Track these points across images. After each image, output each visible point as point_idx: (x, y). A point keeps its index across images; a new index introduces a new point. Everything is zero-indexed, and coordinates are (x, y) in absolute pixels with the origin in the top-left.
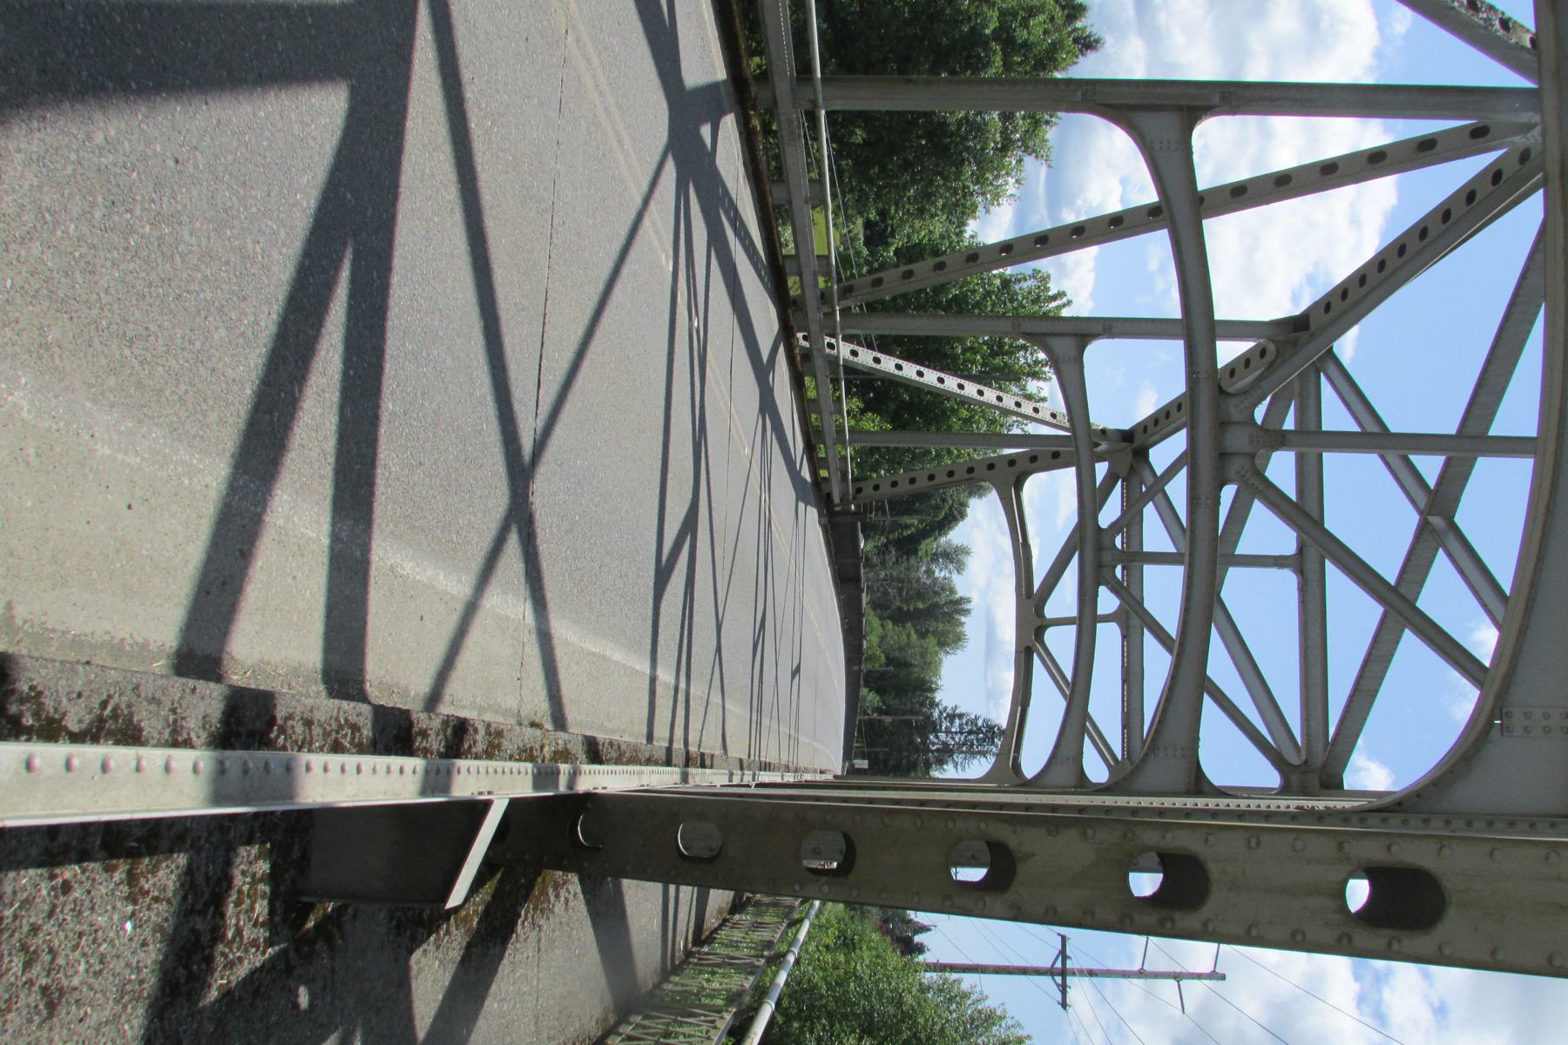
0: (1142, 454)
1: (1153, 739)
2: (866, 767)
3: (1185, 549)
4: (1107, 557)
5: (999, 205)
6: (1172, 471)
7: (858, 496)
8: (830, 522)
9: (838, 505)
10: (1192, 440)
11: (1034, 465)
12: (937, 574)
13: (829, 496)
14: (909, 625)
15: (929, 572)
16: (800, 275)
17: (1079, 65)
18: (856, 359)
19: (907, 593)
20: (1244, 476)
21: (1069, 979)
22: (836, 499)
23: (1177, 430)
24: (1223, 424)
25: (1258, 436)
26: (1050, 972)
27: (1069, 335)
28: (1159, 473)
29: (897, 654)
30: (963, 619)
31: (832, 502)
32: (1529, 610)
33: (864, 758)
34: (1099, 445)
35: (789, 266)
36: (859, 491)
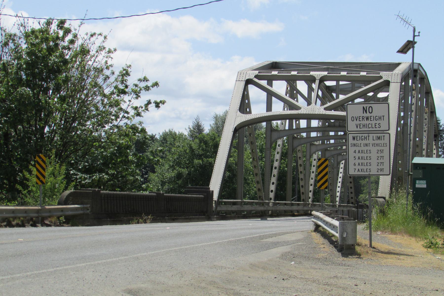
7: (354, 203)
36: (352, 203)
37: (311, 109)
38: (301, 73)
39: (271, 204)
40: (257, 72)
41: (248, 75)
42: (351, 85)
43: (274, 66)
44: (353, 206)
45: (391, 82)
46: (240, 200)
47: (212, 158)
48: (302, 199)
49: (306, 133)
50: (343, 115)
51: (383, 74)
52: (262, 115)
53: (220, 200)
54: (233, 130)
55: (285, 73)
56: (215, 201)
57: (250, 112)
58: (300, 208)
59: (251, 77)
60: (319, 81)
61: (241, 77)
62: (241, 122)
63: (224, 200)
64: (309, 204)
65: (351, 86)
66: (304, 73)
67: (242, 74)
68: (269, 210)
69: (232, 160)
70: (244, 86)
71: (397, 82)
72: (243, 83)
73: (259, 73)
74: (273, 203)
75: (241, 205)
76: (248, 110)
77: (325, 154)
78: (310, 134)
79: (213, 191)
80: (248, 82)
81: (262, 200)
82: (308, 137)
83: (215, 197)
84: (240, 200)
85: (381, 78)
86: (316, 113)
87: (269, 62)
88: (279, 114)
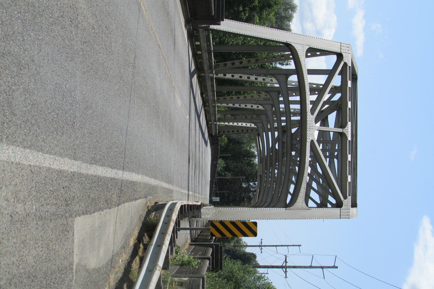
1: (310, 51)
2: (219, 200)
5: (272, 283)
7: (219, 134)
21: (288, 269)
26: (282, 267)
29: (234, 136)
32: (341, 179)
33: (217, 196)
37: (312, 126)
38: (349, 112)
39: (211, 75)
40: (349, 64)
41: (347, 56)
42: (329, 140)
43: (354, 78)
45: (341, 209)
47: (258, 4)
49: (283, 100)
50: (306, 161)
51: (349, 198)
52: (306, 79)
53: (210, 31)
54: (289, 43)
55: (349, 95)
56: (209, 27)
57: (307, 56)
58: (210, 97)
59: (345, 59)
60: (342, 131)
61: (345, 48)
62: (297, 51)
63: (211, 35)
64: (215, 103)
65: (327, 140)
66: (349, 115)
67: (348, 49)
68: (205, 74)
69: (257, 21)
70: (335, 51)
71: (340, 215)
72: (338, 51)
73: (349, 67)
74: (213, 77)
76: (309, 54)
77: (264, 114)
78: (283, 104)
79: (220, 24)
80: (340, 56)
81: (215, 68)
82: (280, 102)
83: (212, 27)
85: (345, 198)
86: (308, 132)
87: (357, 72)
88: (306, 91)
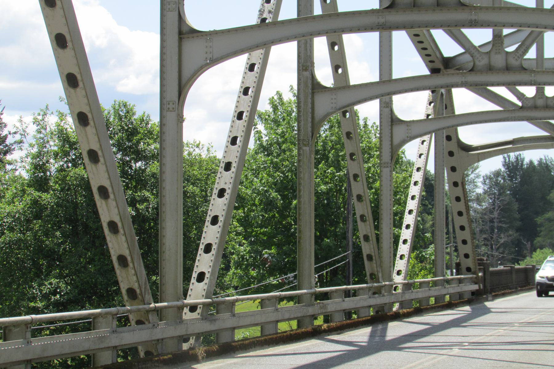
0: (448, 62)
3: (547, 65)
4: (540, 102)
6: (462, 40)
7: (473, 270)
8: (491, 293)
9: (479, 286)
10: (436, 26)
11: (453, 138)
12: (480, 191)
13: (473, 293)
14: (539, 220)
15: (478, 199)
16: (234, 329)
17: (125, 100)
18: (403, 272)
19: (505, 223)
20: (518, 57)
22: (475, 287)
23: (431, 36)
24: (490, 69)
25: (496, 50)
27: (392, 129)
28: (462, 51)
30: (536, 163)
31: (477, 290)
34: (442, 93)
35: (269, 330)
36: (469, 270)
44: (471, 278)
46: (442, 278)
48: (368, 271)
75: (443, 285)
84: (442, 278)
